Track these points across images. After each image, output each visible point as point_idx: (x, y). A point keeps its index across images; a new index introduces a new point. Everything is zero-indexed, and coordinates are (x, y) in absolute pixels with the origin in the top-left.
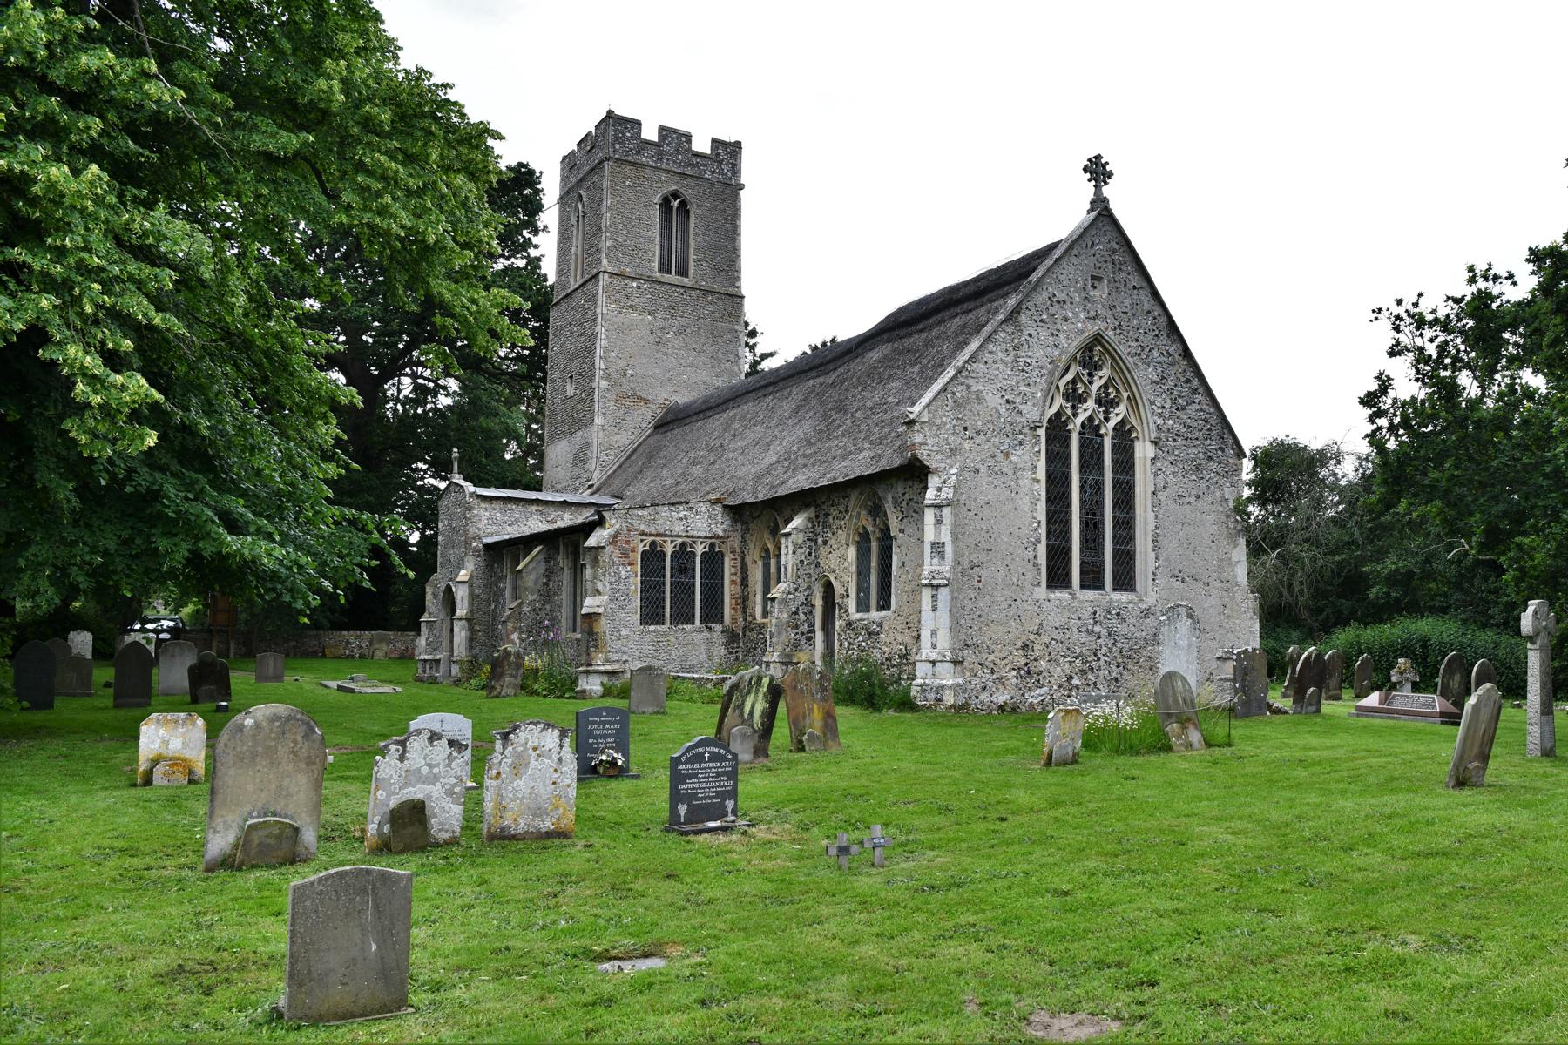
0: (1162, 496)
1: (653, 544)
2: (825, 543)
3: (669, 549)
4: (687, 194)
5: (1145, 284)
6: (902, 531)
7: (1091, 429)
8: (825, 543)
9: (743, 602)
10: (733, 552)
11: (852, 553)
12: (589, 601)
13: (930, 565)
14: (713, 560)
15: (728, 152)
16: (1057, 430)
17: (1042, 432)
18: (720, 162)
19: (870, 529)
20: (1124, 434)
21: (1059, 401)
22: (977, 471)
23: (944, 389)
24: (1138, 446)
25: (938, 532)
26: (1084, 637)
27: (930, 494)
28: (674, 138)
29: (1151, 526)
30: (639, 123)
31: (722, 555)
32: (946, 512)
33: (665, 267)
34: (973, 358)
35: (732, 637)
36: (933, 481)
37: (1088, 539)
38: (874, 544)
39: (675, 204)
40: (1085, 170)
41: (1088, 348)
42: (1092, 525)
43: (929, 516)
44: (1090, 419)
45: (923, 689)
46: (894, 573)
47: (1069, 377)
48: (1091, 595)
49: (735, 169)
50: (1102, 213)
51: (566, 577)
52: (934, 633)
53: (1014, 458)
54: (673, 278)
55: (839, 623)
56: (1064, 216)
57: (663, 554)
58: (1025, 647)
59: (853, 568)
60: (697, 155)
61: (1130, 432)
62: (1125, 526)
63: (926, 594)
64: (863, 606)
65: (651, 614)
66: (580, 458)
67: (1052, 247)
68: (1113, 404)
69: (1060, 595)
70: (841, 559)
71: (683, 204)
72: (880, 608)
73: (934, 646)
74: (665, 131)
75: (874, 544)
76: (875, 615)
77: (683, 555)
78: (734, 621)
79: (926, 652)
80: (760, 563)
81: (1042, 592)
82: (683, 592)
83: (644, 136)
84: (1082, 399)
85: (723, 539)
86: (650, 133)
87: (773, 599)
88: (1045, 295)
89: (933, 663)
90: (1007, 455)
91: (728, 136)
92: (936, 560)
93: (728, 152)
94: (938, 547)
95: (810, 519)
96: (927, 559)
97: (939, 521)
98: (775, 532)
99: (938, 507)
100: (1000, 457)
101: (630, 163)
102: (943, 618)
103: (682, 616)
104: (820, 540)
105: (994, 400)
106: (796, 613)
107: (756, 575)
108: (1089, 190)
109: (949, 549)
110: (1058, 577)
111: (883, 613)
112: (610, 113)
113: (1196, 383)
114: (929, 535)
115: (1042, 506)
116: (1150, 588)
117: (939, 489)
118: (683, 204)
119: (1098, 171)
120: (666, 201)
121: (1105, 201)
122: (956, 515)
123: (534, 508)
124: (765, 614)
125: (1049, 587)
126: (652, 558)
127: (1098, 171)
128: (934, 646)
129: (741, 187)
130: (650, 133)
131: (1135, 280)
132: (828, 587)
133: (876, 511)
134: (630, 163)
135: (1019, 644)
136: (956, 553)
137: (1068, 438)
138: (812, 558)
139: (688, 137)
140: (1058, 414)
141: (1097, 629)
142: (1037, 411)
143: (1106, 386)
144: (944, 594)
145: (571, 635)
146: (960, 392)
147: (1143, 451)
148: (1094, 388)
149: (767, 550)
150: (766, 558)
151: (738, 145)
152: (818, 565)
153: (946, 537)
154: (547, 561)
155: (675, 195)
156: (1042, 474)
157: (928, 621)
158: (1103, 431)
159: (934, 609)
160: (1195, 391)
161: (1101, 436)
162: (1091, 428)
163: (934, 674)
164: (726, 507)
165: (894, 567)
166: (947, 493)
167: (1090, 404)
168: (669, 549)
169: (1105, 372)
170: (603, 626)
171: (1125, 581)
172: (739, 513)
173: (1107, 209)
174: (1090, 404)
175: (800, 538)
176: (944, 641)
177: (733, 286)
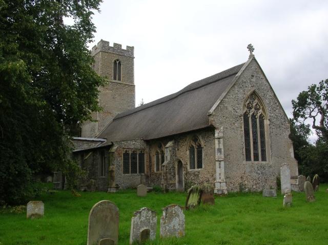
0: (272, 134)
1: (126, 151)
2: (178, 150)
3: (130, 152)
4: (120, 59)
5: (264, 78)
6: (205, 146)
7: (254, 116)
8: (178, 150)
9: (150, 167)
10: (147, 153)
11: (188, 152)
12: (111, 167)
13: (217, 156)
14: (142, 155)
15: (131, 49)
16: (246, 116)
17: (242, 117)
18: (129, 52)
19: (194, 145)
20: (261, 117)
21: (246, 109)
22: (227, 128)
23: (218, 106)
24: (265, 121)
25: (219, 146)
26: (255, 174)
27: (216, 135)
28: (118, 46)
29: (270, 143)
30: (109, 42)
31: (144, 154)
32: (221, 140)
33: (115, 79)
34: (225, 97)
35: (147, 177)
36: (217, 132)
37: (255, 146)
38: (196, 150)
39: (118, 62)
40: (248, 48)
41: (252, 95)
42: (255, 143)
43: (216, 141)
44: (253, 114)
45: (218, 190)
46: (203, 157)
47: (248, 102)
48: (256, 162)
49: (132, 54)
50: (253, 60)
51: (99, 161)
52: (220, 174)
53: (236, 125)
54: (117, 81)
55: (184, 172)
56: (244, 58)
57: (128, 154)
58: (242, 177)
59: (188, 157)
60: (123, 50)
61: (263, 117)
62: (263, 143)
63: (217, 163)
64: (193, 167)
65: (126, 171)
66: (93, 130)
67: (242, 65)
68: (258, 109)
69: (249, 162)
70: (184, 154)
71: (120, 62)
72: (198, 168)
73: (220, 178)
74: (115, 44)
75: (196, 150)
76: (196, 169)
77: (134, 154)
78: (148, 172)
79: (218, 180)
80: (155, 156)
81: (245, 162)
82: (134, 164)
83: (110, 46)
84: (251, 109)
85: (144, 150)
86: (111, 45)
87: (164, 166)
88: (241, 81)
89: (220, 183)
90: (234, 124)
91: (131, 45)
92: (219, 154)
93: (131, 49)
94: (219, 150)
95: (173, 143)
96: (216, 154)
97: (219, 143)
98: (160, 147)
99: (219, 138)
100: (232, 124)
101: (106, 52)
102: (223, 170)
103: (134, 171)
104: (176, 149)
105: (230, 109)
106: (170, 170)
107: (154, 159)
108: (249, 53)
109: (223, 150)
110: (248, 158)
111: (199, 169)
112: (102, 40)
113: (277, 104)
114: (217, 147)
115: (244, 138)
116: (270, 161)
117: (219, 133)
118: (120, 62)
119: (251, 48)
120: (115, 62)
121: (254, 55)
122: (223, 140)
123: (85, 142)
124: (158, 169)
125: (246, 160)
126: (126, 154)
127: (251, 48)
128: (220, 178)
129: (134, 58)
130: (111, 45)
131: (262, 76)
132: (180, 162)
133: (195, 140)
134: (106, 52)
135: (240, 177)
136: (224, 151)
137: (248, 119)
138: (174, 154)
139: (121, 45)
140: (246, 113)
141: (259, 172)
142: (241, 112)
143: (256, 105)
144: (222, 163)
145: (101, 177)
146: (222, 106)
147: (266, 122)
148: (254, 105)
149: (157, 152)
150: (157, 154)
151: (133, 47)
152: (176, 156)
153: (222, 147)
154: (93, 156)
155: (118, 60)
156: (243, 129)
157: (218, 170)
158: (256, 117)
159: (220, 167)
160: (277, 106)
161: (256, 118)
162: (254, 116)
163: (220, 186)
164: (145, 141)
165: (203, 156)
166: (221, 135)
167: (253, 109)
168: (130, 152)
169: (256, 101)
170: (115, 174)
171: (264, 159)
172: (149, 142)
173: (254, 58)
174: (253, 109)
175: (171, 149)
176: (223, 177)
177: (132, 83)
